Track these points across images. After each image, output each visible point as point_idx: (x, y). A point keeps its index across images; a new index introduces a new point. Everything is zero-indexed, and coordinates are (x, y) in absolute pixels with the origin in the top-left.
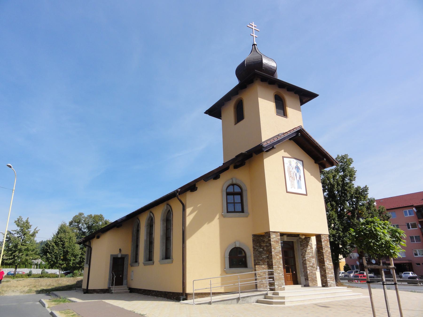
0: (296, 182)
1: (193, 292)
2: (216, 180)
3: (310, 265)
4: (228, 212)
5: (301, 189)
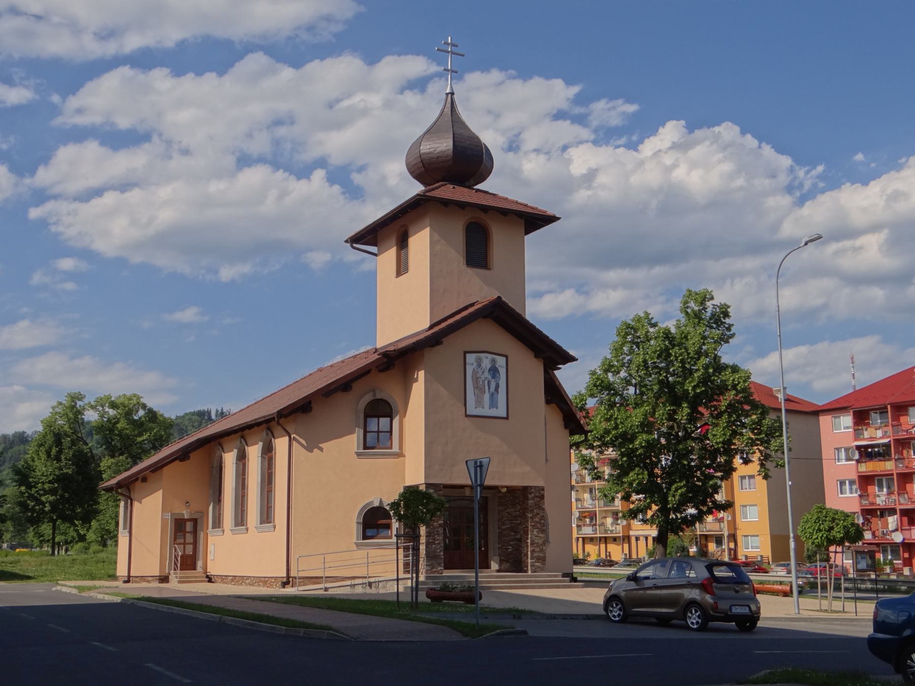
0: (487, 397)
1: (822, 600)
2: (307, 413)
3: (516, 537)
4: (365, 448)
5: (497, 408)
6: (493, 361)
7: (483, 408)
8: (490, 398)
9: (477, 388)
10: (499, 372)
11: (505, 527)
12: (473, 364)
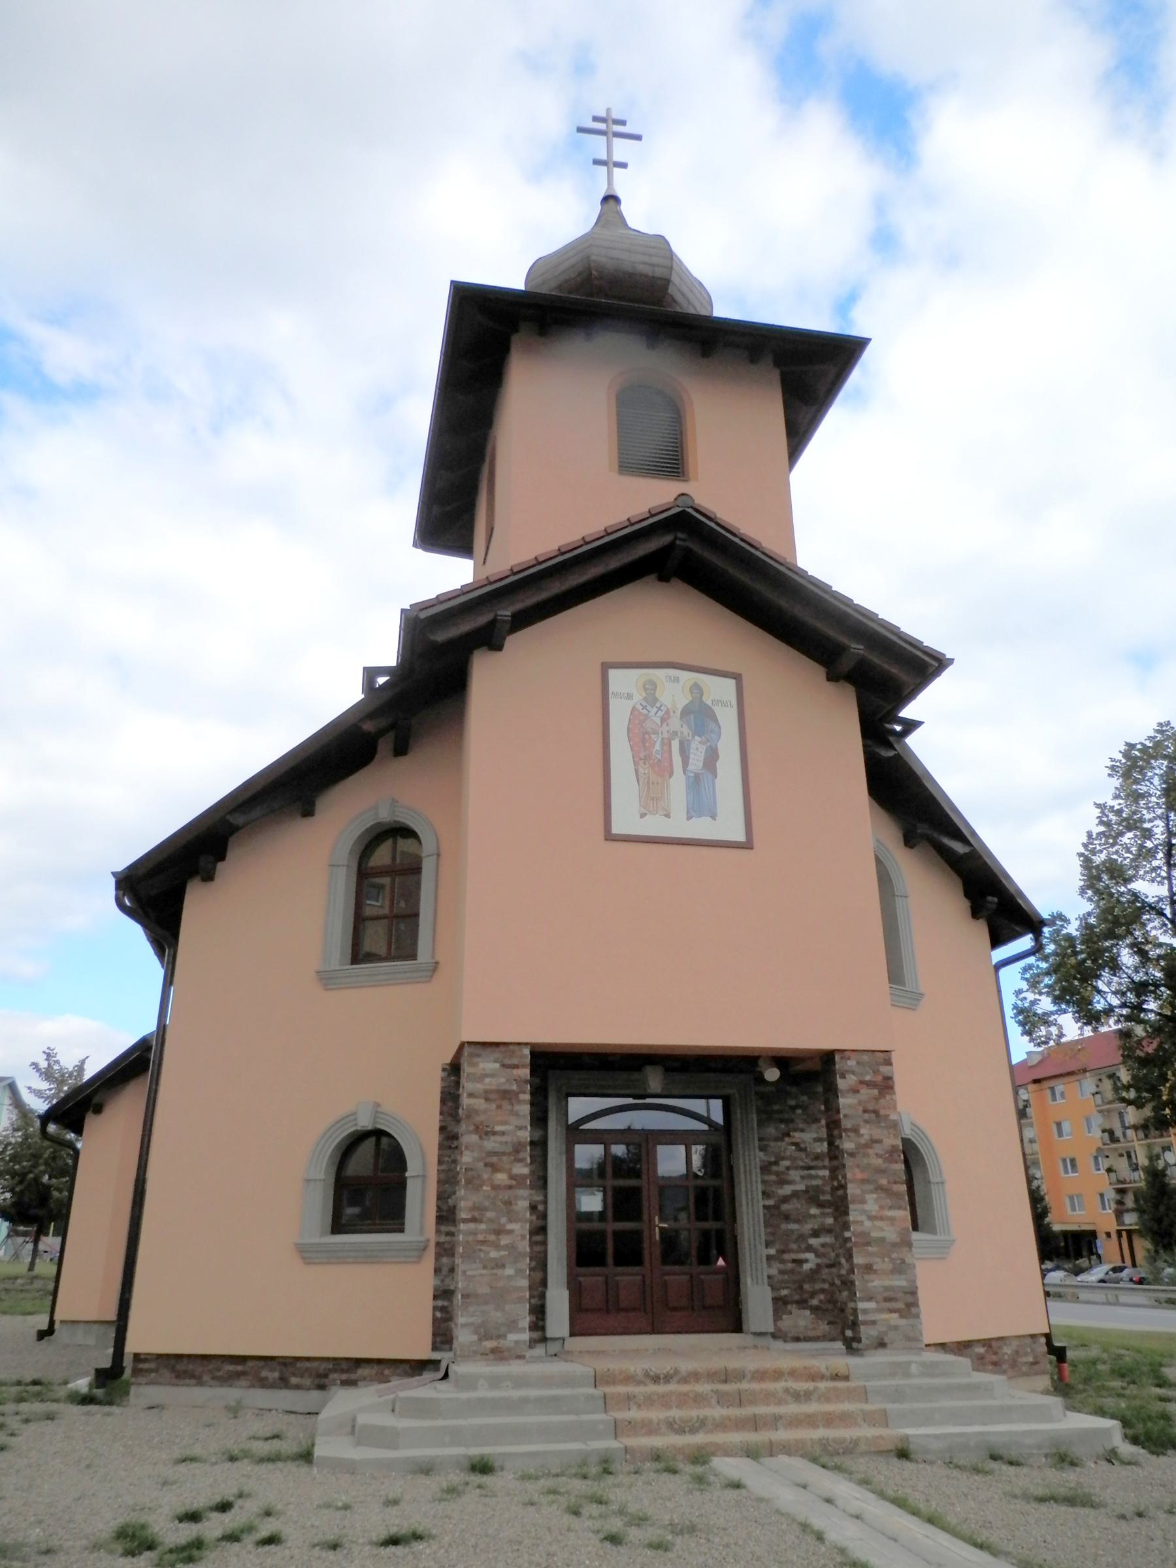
0: (678, 785)
5: (714, 817)
6: (696, 689)
7: (668, 816)
8: (688, 787)
9: (646, 758)
10: (716, 721)
11: (787, 1190)
12: (630, 696)
